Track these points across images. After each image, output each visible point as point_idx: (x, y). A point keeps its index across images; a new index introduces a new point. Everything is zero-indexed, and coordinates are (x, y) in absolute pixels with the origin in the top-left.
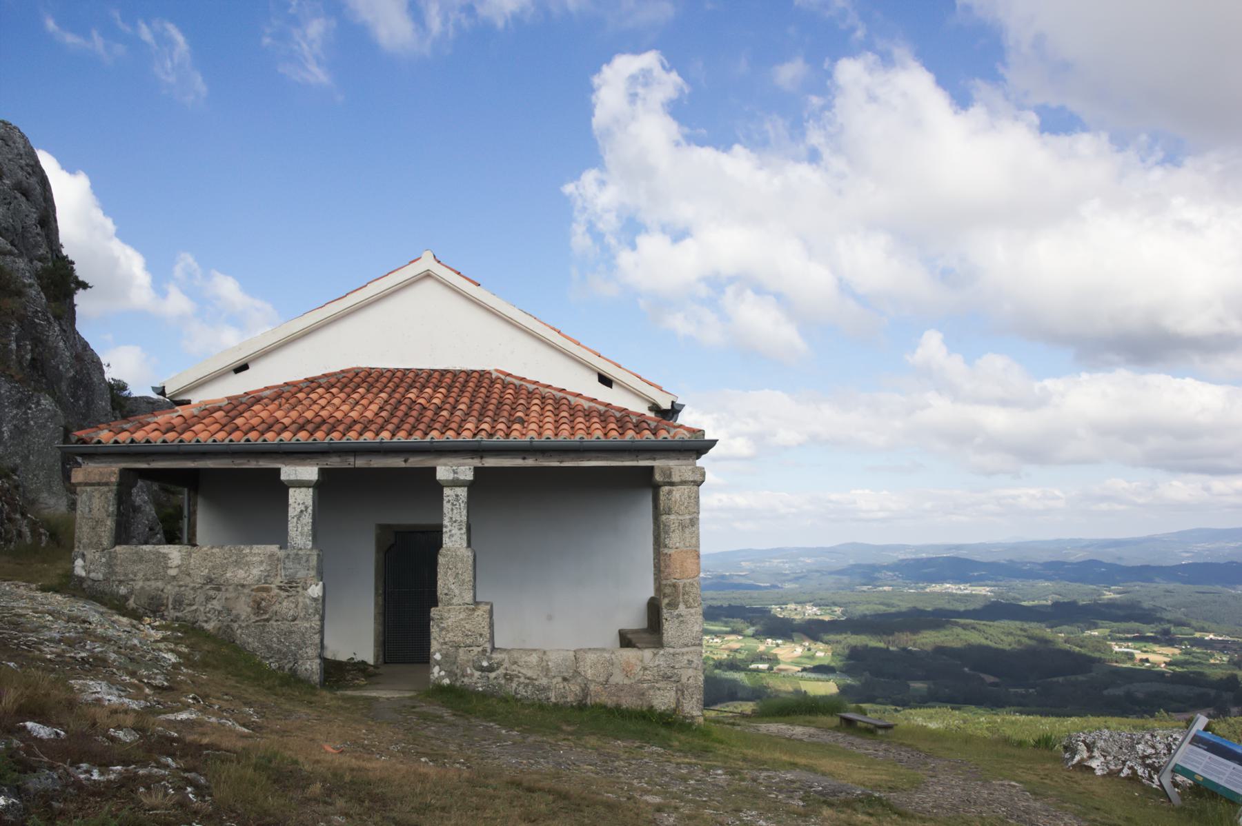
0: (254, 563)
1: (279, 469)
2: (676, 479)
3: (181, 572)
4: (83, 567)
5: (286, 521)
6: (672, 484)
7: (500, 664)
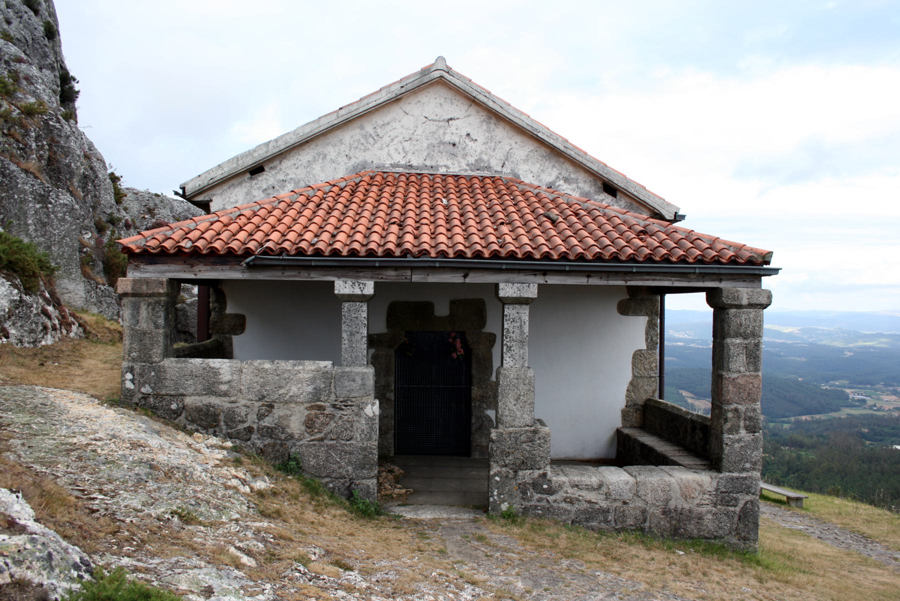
0: (301, 375)
1: (333, 282)
2: (745, 302)
3: (231, 387)
4: (132, 381)
5: (340, 338)
6: (739, 307)
7: (560, 486)
